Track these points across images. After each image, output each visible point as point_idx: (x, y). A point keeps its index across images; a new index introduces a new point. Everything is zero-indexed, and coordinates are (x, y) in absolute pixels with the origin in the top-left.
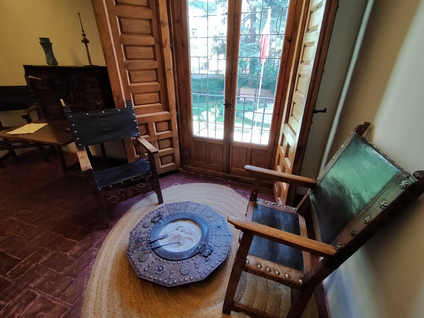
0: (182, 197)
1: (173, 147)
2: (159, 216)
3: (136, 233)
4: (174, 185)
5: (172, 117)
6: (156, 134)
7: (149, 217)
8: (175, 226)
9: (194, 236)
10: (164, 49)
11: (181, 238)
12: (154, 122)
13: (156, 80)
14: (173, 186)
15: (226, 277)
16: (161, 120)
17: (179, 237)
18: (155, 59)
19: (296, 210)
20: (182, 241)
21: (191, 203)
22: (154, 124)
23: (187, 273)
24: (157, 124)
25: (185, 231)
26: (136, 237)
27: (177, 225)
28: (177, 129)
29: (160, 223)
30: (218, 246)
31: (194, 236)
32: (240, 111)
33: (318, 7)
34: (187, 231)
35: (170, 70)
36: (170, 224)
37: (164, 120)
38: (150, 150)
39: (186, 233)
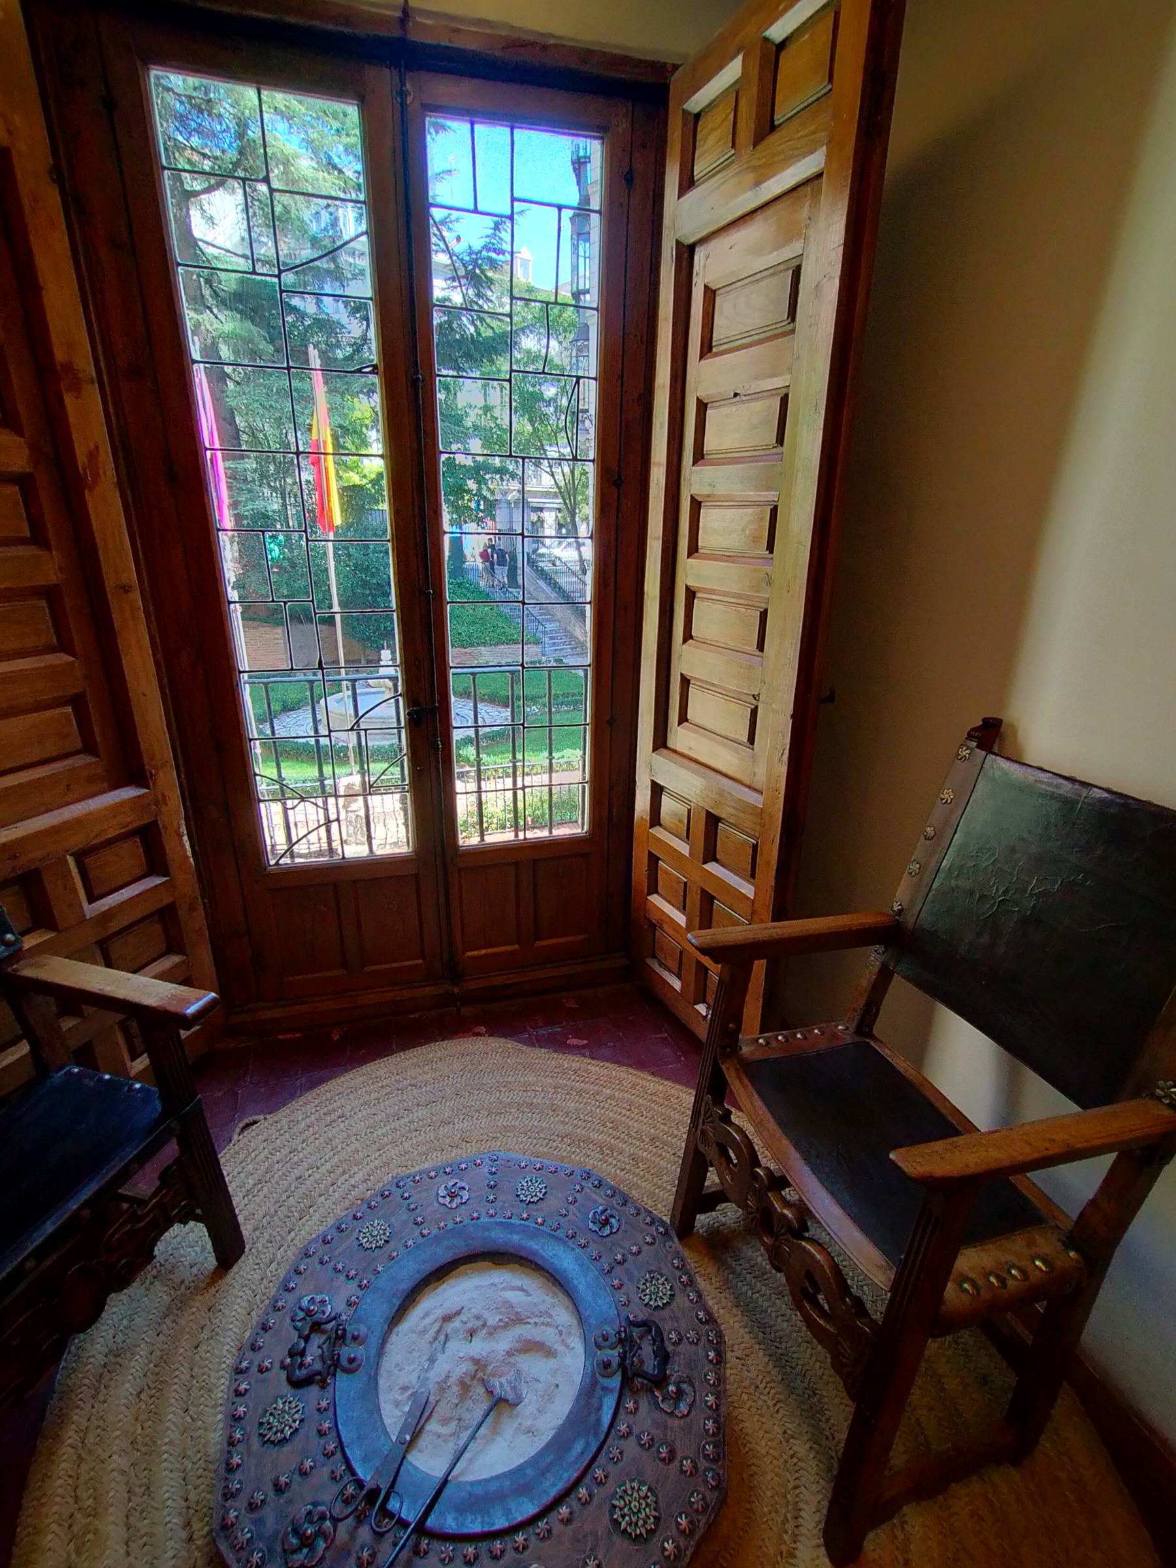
0: (323, 1169)
1: (180, 950)
2: (317, 1327)
3: (252, 1507)
4: (238, 1130)
5: (164, 809)
6: (91, 910)
7: (267, 1369)
8: (424, 1332)
9: (537, 1320)
10: (86, 492)
11: (490, 1368)
12: (71, 855)
13: (55, 640)
14: (235, 1137)
15: (741, 1413)
16: (111, 834)
17: (480, 1374)
18: (38, 538)
19: (847, 1029)
20: (503, 1380)
21: (417, 1178)
22: (70, 859)
23: (655, 1517)
24: (89, 861)
25: (484, 1325)
26: (277, 1533)
27: (432, 1317)
28: (188, 857)
29: (351, 1360)
30: (663, 1304)
31: (537, 1320)
32: (573, 732)
33: (736, 395)
34: (492, 1320)
35: (126, 589)
36: (393, 1338)
37: (123, 830)
38: (170, 1008)
39: (493, 1332)
